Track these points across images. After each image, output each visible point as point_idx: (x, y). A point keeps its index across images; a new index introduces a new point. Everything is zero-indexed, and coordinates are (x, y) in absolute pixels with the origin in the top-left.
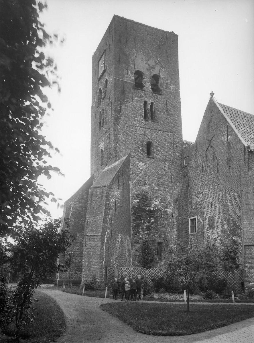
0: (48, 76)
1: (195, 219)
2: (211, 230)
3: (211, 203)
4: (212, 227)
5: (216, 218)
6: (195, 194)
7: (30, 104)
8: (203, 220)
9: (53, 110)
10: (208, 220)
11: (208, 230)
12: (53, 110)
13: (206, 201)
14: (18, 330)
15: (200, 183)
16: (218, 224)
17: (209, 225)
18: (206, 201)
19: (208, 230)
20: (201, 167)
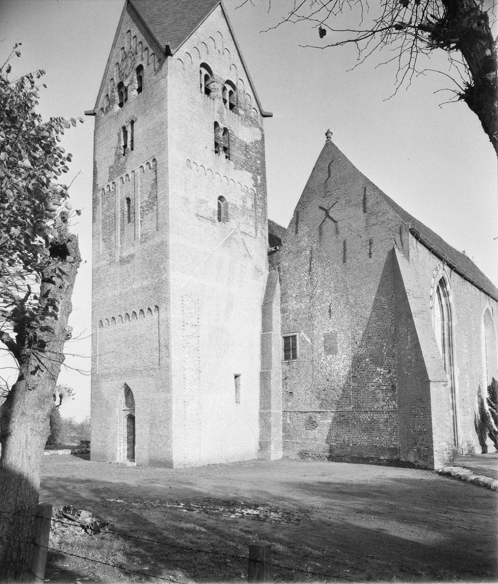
0: (411, 19)
1: (295, 336)
2: (331, 356)
3: (330, 311)
4: (330, 350)
5: (341, 336)
6: (294, 295)
7: (439, 48)
8: (311, 339)
9: (20, 44)
10: (323, 339)
11: (323, 355)
12: (20, 44)
13: (319, 307)
14: (258, 534)
15: (306, 278)
16: (345, 346)
17: (325, 347)
18: (319, 307)
19: (323, 355)
20: (308, 252)
